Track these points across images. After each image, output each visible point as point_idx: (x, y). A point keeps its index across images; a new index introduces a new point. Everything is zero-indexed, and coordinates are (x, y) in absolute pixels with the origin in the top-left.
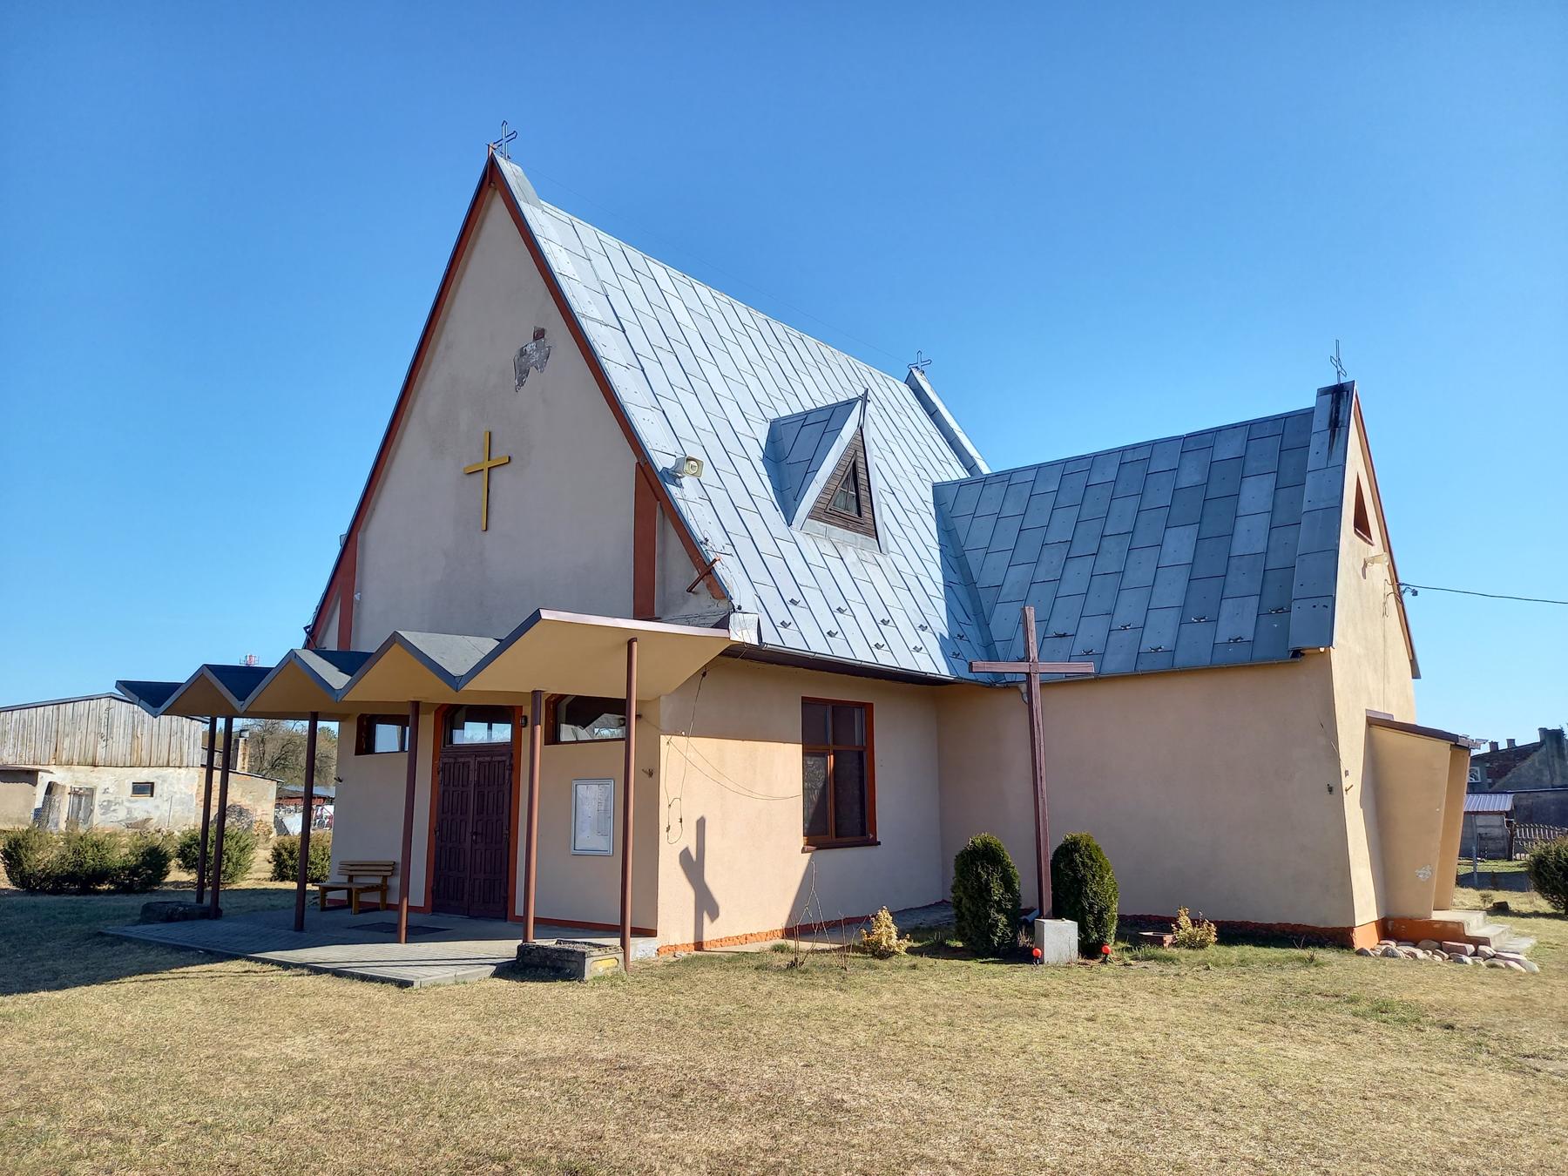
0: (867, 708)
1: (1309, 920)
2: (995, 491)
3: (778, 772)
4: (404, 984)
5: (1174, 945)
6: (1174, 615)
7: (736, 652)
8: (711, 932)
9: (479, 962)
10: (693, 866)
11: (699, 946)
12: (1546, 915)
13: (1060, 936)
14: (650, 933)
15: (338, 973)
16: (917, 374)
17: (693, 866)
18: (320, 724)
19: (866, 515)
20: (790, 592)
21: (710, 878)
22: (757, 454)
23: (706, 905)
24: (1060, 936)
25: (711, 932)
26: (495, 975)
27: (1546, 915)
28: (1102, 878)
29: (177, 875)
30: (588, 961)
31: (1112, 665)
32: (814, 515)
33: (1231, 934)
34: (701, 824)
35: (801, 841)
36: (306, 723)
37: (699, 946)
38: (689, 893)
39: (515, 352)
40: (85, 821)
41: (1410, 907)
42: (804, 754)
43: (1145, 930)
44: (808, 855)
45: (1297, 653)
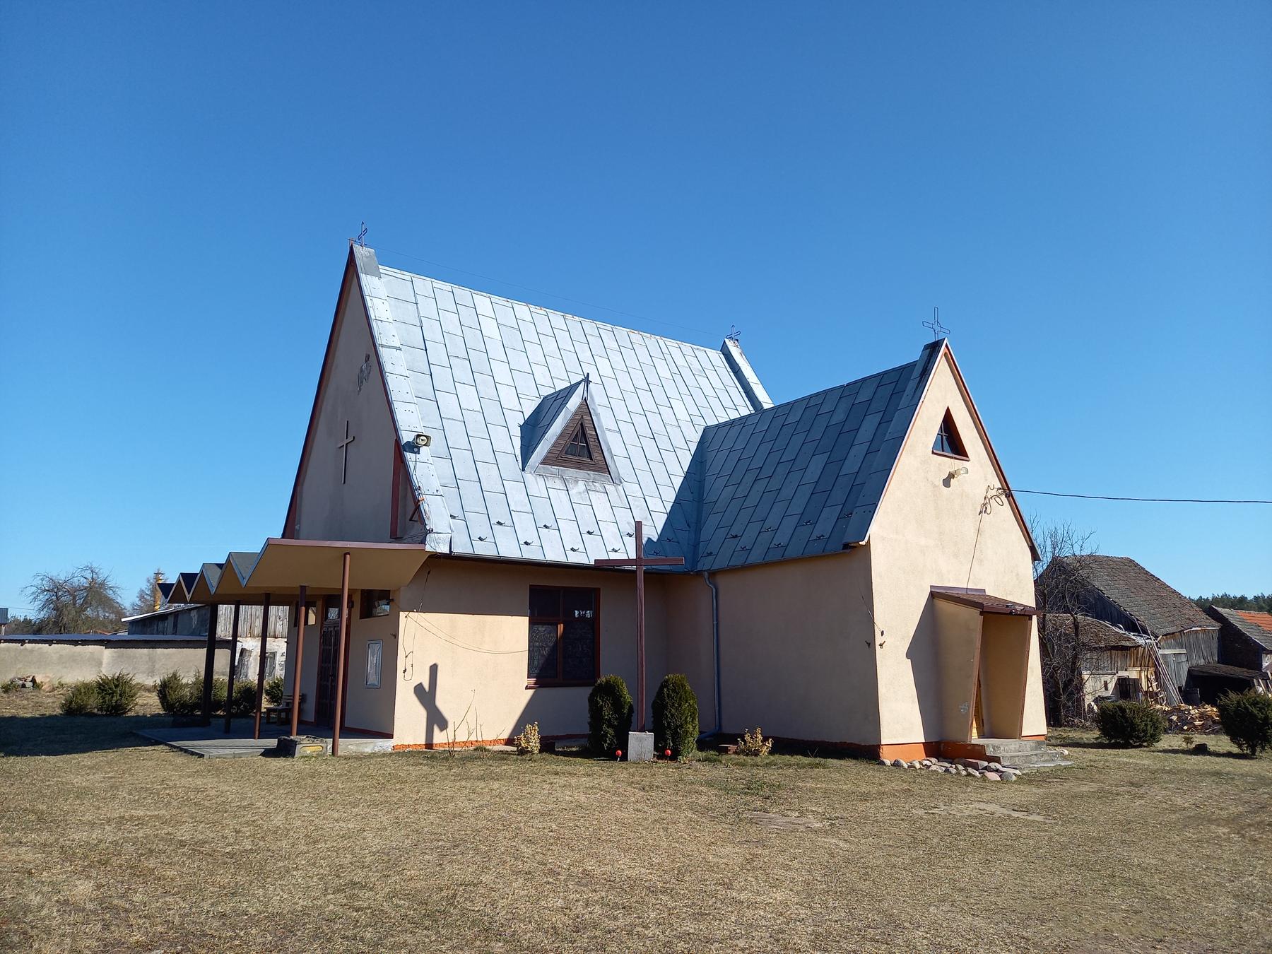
0: (597, 591)
1: (836, 738)
2: (737, 429)
3: (509, 635)
4: (202, 756)
5: (735, 753)
6: (796, 518)
7: (435, 557)
8: (439, 737)
9: (253, 747)
10: (426, 696)
11: (429, 745)
12: (1229, 755)
13: (641, 742)
14: (391, 736)
15: (186, 751)
16: (730, 344)
17: (426, 696)
18: (242, 608)
19: (595, 455)
20: (499, 513)
21: (440, 702)
22: (516, 421)
23: (436, 719)
24: (641, 742)
25: (439, 737)
26: (262, 755)
27: (1229, 755)
28: (680, 705)
29: (265, 704)
30: (298, 747)
31: (755, 557)
32: (546, 461)
33: (784, 746)
34: (434, 669)
35: (525, 680)
36: (233, 607)
37: (429, 745)
38: (421, 713)
39: (358, 371)
40: (270, 674)
41: (953, 735)
42: (532, 623)
43: (716, 741)
44: (531, 692)
45: (846, 546)
